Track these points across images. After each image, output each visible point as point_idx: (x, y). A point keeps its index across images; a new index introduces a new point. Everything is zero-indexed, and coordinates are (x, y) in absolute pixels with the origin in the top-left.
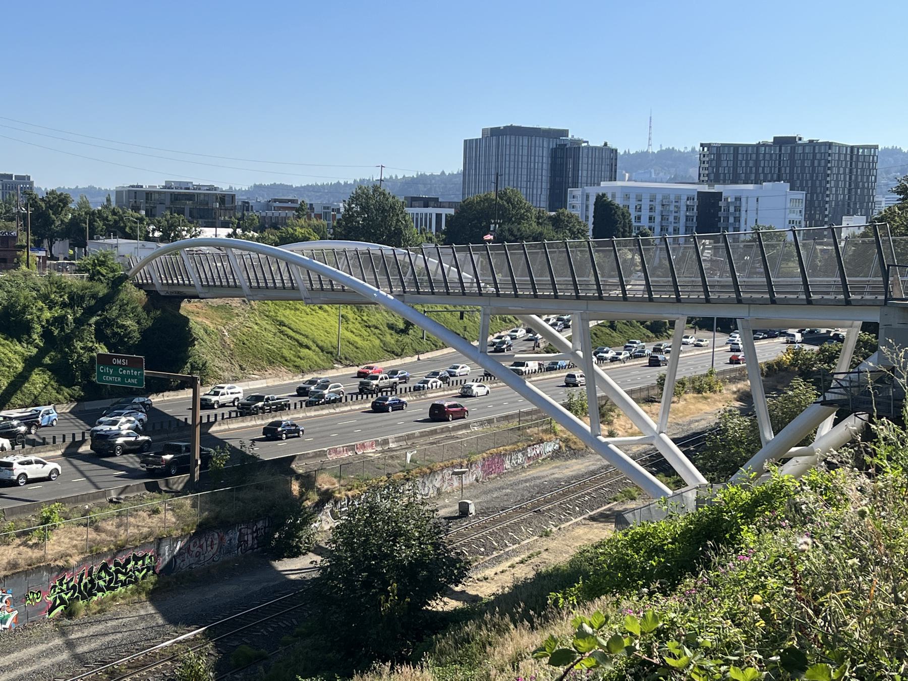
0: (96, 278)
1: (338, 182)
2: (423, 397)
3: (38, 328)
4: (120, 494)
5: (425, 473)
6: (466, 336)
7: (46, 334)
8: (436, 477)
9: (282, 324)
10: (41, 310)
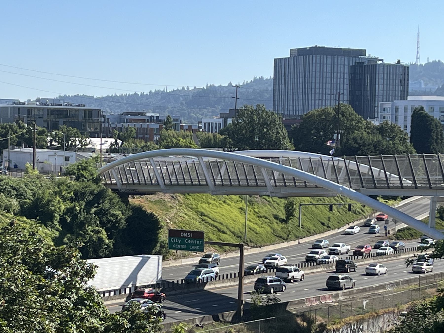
0: (81, 180)
1: (136, 94)
2: (331, 268)
3: (57, 217)
4: (201, 322)
5: (374, 316)
6: (329, 225)
7: (62, 221)
8: (380, 320)
9: (202, 214)
10: (59, 202)
